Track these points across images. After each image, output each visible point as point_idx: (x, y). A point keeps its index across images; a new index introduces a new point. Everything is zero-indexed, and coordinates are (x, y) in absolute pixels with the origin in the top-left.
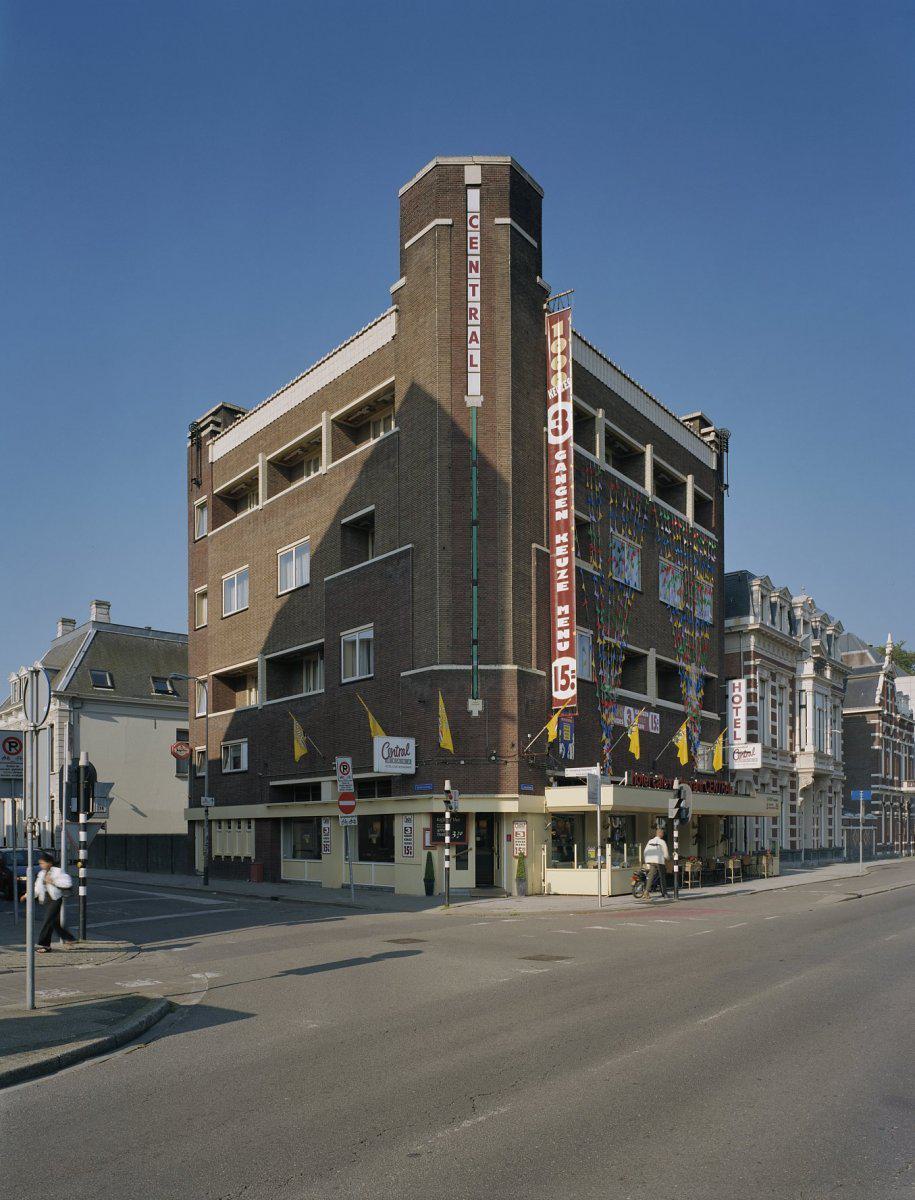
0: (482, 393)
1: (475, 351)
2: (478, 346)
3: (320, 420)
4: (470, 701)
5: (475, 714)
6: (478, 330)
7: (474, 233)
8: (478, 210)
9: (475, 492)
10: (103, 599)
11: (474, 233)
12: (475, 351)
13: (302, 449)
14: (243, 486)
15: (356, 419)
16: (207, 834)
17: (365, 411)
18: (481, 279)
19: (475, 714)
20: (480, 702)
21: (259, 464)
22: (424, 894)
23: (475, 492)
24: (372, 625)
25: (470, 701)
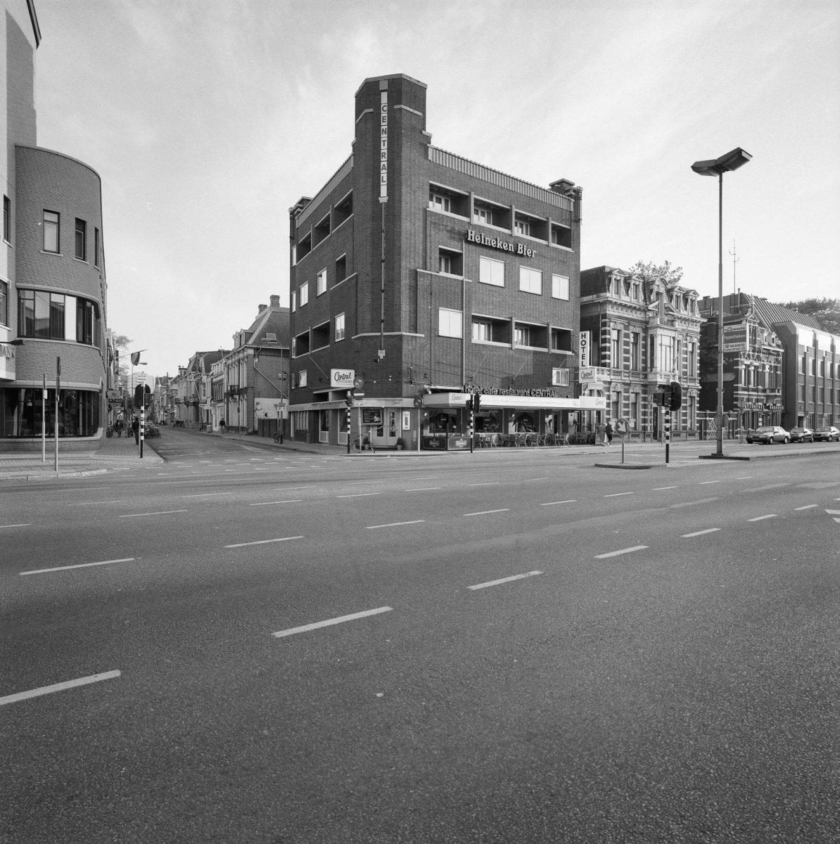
4: (379, 351)
5: (381, 357)
6: (386, 163)
7: (384, 114)
11: (384, 114)
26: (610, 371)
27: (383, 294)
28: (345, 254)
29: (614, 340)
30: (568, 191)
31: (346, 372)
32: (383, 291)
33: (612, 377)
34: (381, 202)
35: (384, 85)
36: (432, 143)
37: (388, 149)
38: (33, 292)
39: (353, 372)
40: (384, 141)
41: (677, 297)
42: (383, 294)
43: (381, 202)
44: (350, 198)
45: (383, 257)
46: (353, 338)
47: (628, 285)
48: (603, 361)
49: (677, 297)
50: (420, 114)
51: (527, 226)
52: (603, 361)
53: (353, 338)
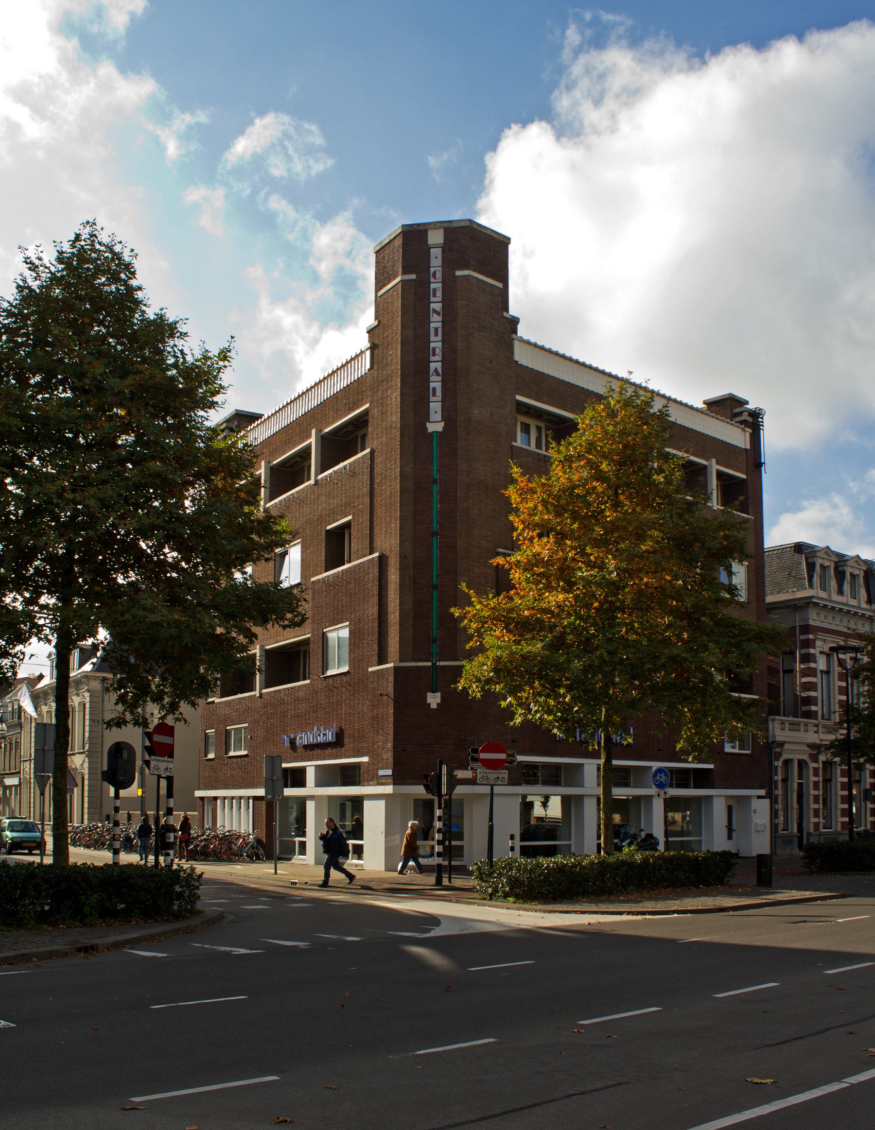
0: (443, 419)
1: (436, 383)
2: (440, 378)
3: (310, 436)
4: (429, 695)
5: (434, 706)
6: (439, 366)
7: (436, 285)
8: (441, 265)
9: (436, 506)
10: (631, 371)
11: (436, 285)
12: (436, 383)
13: (301, 457)
14: (297, 459)
15: (291, 466)
16: (304, 874)
17: (350, 428)
18: (443, 322)
19: (434, 706)
20: (439, 694)
21: (312, 440)
22: (383, 869)
23: (436, 506)
24: (347, 623)
25: (429, 695)
26: (816, 726)
27: (435, 592)
28: (350, 518)
29: (822, 672)
30: (740, 414)
31: (504, 771)
32: (435, 587)
33: (822, 736)
34: (430, 431)
35: (436, 238)
36: (519, 334)
37: (444, 341)
38: (495, 798)
39: (507, 772)
40: (436, 329)
41: (853, 576)
42: (435, 592)
43: (430, 431)
44: (361, 422)
45: (435, 527)
46: (370, 669)
47: (840, 576)
48: (805, 708)
49: (853, 576)
50: (500, 285)
51: (539, 429)
52: (805, 708)
53: (370, 669)
